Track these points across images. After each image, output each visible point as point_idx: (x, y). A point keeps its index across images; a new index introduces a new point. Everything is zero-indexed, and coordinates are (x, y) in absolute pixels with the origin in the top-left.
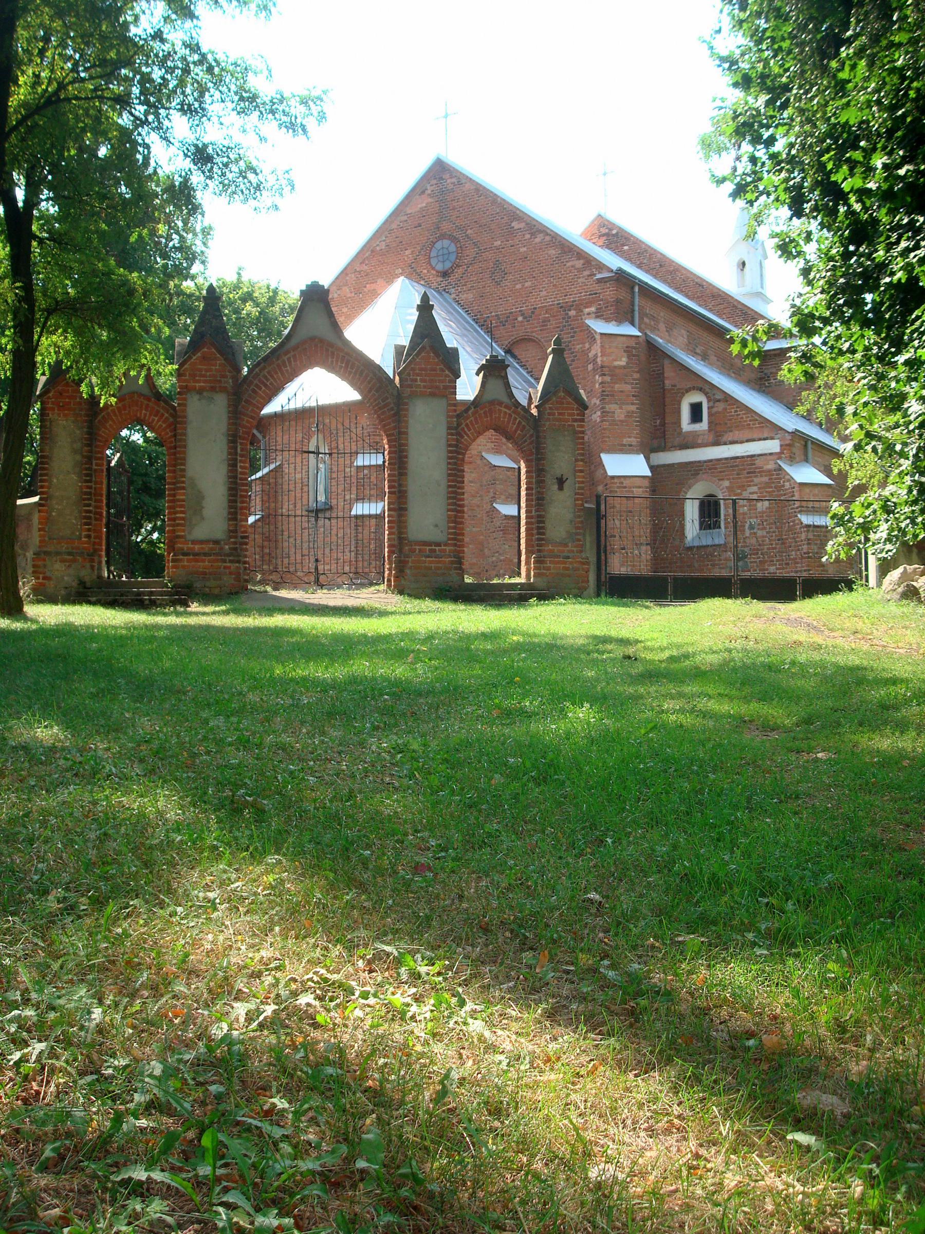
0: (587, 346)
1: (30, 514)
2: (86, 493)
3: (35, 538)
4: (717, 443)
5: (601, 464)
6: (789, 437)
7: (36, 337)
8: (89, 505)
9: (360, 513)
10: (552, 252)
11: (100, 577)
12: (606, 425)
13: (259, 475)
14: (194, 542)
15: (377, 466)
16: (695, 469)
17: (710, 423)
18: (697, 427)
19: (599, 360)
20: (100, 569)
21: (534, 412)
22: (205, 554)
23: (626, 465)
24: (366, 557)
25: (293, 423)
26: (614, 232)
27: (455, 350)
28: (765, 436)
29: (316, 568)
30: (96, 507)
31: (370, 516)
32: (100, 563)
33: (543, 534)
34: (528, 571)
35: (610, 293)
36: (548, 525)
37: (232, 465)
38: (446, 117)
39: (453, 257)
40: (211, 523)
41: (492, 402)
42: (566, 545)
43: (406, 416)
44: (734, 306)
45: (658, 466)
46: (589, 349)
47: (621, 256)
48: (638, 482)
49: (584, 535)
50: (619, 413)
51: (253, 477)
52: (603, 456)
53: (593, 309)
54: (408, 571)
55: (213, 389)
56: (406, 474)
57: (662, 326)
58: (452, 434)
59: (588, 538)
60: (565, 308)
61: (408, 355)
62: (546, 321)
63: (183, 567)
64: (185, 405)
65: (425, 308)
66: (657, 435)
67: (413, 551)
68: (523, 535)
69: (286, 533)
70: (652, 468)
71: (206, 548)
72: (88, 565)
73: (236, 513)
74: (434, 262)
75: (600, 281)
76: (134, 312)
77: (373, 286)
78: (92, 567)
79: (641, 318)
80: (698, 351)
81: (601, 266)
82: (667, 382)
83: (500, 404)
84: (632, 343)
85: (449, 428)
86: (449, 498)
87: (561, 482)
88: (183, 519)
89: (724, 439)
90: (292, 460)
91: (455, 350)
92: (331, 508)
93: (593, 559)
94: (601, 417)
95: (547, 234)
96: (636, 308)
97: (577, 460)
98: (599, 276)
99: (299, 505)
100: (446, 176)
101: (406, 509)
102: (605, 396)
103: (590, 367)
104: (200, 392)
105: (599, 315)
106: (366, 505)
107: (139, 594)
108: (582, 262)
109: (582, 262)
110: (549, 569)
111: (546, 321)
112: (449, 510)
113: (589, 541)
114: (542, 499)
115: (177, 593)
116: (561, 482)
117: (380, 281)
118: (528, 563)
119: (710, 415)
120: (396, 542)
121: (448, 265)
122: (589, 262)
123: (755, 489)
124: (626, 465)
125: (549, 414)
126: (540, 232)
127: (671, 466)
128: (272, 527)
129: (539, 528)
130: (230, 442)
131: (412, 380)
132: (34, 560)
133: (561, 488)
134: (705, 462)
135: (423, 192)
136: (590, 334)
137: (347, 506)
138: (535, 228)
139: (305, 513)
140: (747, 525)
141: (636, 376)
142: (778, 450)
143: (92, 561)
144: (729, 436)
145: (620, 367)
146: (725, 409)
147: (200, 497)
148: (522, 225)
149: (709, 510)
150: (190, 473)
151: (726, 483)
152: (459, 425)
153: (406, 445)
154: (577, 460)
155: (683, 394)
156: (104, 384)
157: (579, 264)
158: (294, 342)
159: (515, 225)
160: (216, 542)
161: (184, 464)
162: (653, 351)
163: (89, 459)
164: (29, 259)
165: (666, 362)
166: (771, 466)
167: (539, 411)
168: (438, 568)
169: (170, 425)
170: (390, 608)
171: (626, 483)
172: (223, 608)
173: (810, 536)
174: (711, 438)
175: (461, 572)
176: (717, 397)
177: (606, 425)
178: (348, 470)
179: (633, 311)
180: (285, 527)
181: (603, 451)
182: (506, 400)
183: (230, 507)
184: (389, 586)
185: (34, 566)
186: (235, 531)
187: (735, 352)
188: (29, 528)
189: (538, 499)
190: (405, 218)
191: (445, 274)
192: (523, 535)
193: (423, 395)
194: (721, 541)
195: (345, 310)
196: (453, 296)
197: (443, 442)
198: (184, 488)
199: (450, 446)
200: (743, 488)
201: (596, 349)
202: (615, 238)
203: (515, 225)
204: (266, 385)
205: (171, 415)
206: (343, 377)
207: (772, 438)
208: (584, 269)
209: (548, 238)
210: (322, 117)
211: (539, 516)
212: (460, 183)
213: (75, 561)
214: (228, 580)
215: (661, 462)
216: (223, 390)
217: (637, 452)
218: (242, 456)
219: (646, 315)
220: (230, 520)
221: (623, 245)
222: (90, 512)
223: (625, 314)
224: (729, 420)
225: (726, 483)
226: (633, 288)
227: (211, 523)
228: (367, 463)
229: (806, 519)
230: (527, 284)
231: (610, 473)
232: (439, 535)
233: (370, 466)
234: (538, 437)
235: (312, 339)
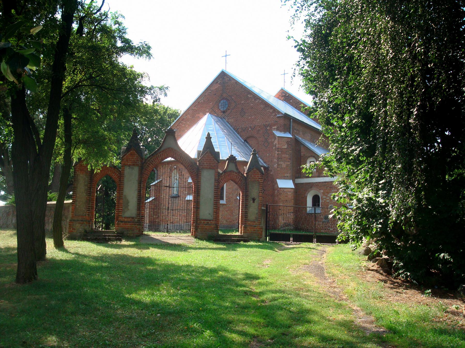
0: (273, 140)
1: (69, 207)
2: (88, 200)
3: (70, 215)
4: (319, 176)
5: (277, 183)
7: (72, 151)
8: (89, 204)
9: (188, 199)
10: (262, 106)
11: (92, 229)
12: (279, 169)
13: (154, 183)
14: (125, 218)
16: (311, 186)
20: (92, 226)
21: (245, 175)
22: (128, 222)
23: (286, 184)
25: (167, 165)
27: (219, 153)
30: (92, 205)
32: (92, 224)
33: (247, 218)
34: (241, 230)
35: (282, 122)
36: (249, 215)
37: (139, 191)
39: (227, 106)
40: (131, 210)
41: (231, 171)
42: (255, 222)
43: (200, 175)
45: (298, 184)
48: (290, 190)
49: (261, 219)
50: (284, 165)
51: (152, 184)
52: (277, 180)
53: (276, 127)
54: (199, 230)
55: (134, 165)
56: (199, 196)
57: (301, 133)
59: (263, 220)
60: (266, 126)
61: (202, 154)
62: (259, 130)
63: (121, 226)
64: (124, 170)
66: (297, 174)
67: (201, 223)
68: (240, 217)
70: (295, 184)
71: (129, 220)
72: (88, 225)
73: (140, 208)
74: (220, 108)
75: (278, 117)
76: (105, 144)
77: (199, 115)
78: (89, 226)
79: (293, 130)
82: (302, 154)
83: (233, 172)
85: (215, 180)
86: (214, 204)
87: (254, 200)
88: (121, 209)
90: (166, 179)
91: (219, 153)
92: (179, 196)
93: (264, 227)
94: (277, 166)
96: (291, 127)
97: (260, 192)
98: (278, 116)
100: (225, 77)
101: (199, 208)
102: (279, 159)
103: (274, 148)
104: (129, 166)
105: (278, 129)
107: (105, 236)
110: (248, 230)
111: (259, 130)
113: (263, 221)
114: (247, 206)
115: (118, 236)
116: (254, 200)
117: (201, 113)
118: (241, 228)
120: (195, 219)
121: (225, 109)
122: (275, 110)
124: (286, 184)
126: (258, 99)
127: (302, 184)
128: (158, 202)
129: (245, 216)
130: (139, 183)
132: (69, 222)
133: (254, 202)
135: (217, 83)
138: (256, 97)
141: (290, 152)
143: (90, 223)
145: (285, 148)
147: (128, 202)
148: (252, 96)
149: (316, 200)
150: (124, 194)
151: (322, 191)
152: (219, 179)
153: (200, 186)
154: (260, 192)
155: (307, 159)
156: (96, 166)
157: (271, 111)
158: (162, 149)
159: (249, 96)
160: (133, 218)
161: (123, 191)
162: (297, 142)
163: (90, 188)
164: (71, 123)
165: (302, 146)
167: (247, 175)
168: (210, 229)
169: (118, 177)
170: (190, 245)
171: (285, 190)
172: (133, 243)
174: (317, 174)
175: (218, 230)
177: (279, 169)
179: (290, 128)
180: (162, 202)
181: (277, 178)
182: (235, 171)
183: (138, 206)
184: (192, 235)
185: (69, 225)
186: (139, 214)
187: (304, 172)
188: (68, 211)
189: (246, 206)
190: (210, 91)
191: (224, 112)
192: (240, 217)
193: (207, 168)
195: (188, 123)
197: (213, 185)
198: (122, 199)
199: (215, 186)
201: (276, 142)
203: (249, 96)
204: (152, 164)
205: (119, 174)
206: (183, 152)
208: (273, 113)
209: (260, 101)
210: (166, 95)
211: (246, 212)
212: (230, 80)
213: (83, 223)
214: (136, 231)
215: (299, 182)
216: (137, 165)
217: (290, 179)
218: (143, 188)
219: (295, 129)
220: (138, 210)
222: (89, 206)
223: (286, 129)
225: (322, 191)
226: (290, 120)
227: (131, 210)
231: (280, 187)
232: (210, 217)
234: (246, 184)
235: (169, 148)
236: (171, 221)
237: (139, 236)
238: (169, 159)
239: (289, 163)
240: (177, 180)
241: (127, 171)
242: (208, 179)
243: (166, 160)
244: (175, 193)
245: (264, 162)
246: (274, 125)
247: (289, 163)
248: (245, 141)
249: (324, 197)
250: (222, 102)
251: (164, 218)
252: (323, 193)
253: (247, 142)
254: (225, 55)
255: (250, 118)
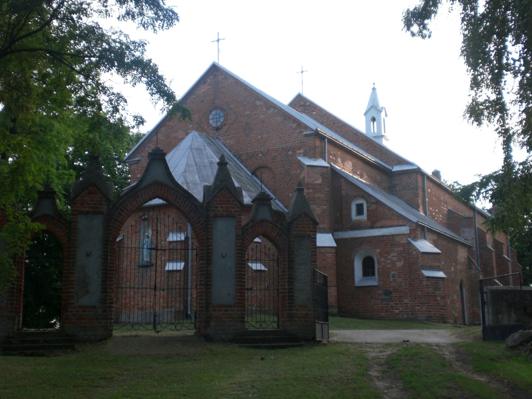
0: (299, 171)
4: (372, 227)
6: (414, 225)
9: (171, 268)
15: (181, 241)
17: (368, 216)
18: (360, 218)
19: (306, 180)
23: (325, 240)
24: (174, 295)
26: (308, 104)
28: (401, 224)
29: (155, 320)
31: (177, 271)
38: (218, 41)
39: (222, 120)
41: (263, 221)
44: (375, 146)
46: (300, 174)
47: (311, 117)
53: (302, 151)
57: (339, 160)
58: (238, 239)
65: (222, 164)
66: (339, 223)
69: (125, 279)
70: (336, 241)
75: (306, 136)
80: (358, 173)
81: (306, 127)
82: (343, 192)
83: (267, 221)
84: (325, 171)
85: (237, 236)
89: (376, 226)
95: (276, 109)
98: (305, 133)
99: (133, 264)
101: (210, 285)
105: (305, 155)
106: (175, 264)
108: (295, 124)
109: (295, 124)
112: (236, 285)
119: (368, 211)
121: (219, 124)
123: (395, 254)
124: (325, 240)
125: (296, 227)
126: (272, 107)
127: (346, 239)
131: (215, 207)
134: (366, 238)
136: (301, 165)
137: (163, 264)
139: (136, 267)
140: (391, 275)
141: (327, 189)
142: (408, 232)
144: (379, 224)
146: (377, 208)
148: (261, 103)
149: (369, 267)
151: (378, 250)
158: (144, 184)
160: (94, 307)
166: (404, 241)
173: (429, 283)
176: (372, 201)
178: (163, 243)
194: (375, 283)
196: (222, 141)
199: (237, 246)
200: (388, 253)
202: (300, 102)
207: (404, 225)
219: (331, 154)
221: (313, 111)
222: (14, 288)
224: (379, 215)
225: (378, 250)
228: (175, 239)
229: (427, 273)
230: (264, 136)
233: (177, 242)
236: (140, 307)
237: (105, 339)
238: (157, 201)
239: (325, 207)
240: (148, 237)
241: (82, 222)
242: (224, 233)
243: (147, 204)
244: (146, 259)
245: (285, 207)
246: (299, 148)
247: (325, 207)
248: (253, 173)
249: (383, 259)
250: (214, 112)
251: (128, 301)
252: (380, 254)
253: (257, 176)
254: (217, 39)
255: (259, 137)
